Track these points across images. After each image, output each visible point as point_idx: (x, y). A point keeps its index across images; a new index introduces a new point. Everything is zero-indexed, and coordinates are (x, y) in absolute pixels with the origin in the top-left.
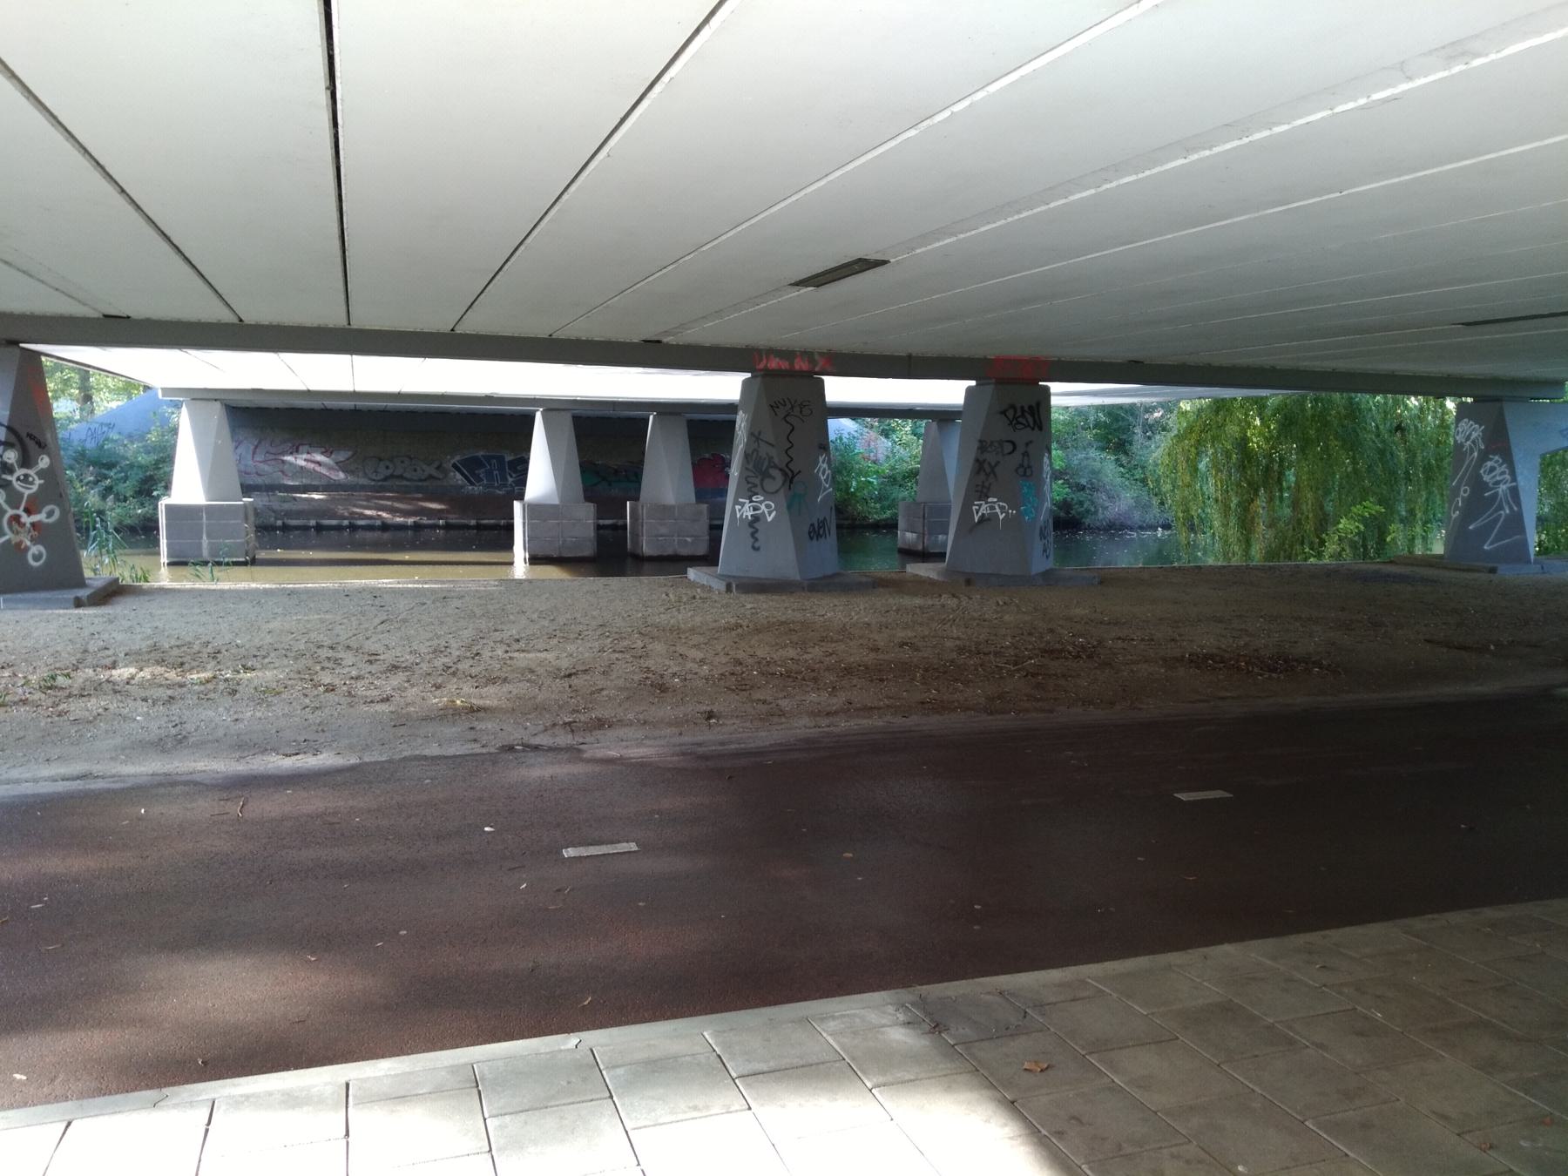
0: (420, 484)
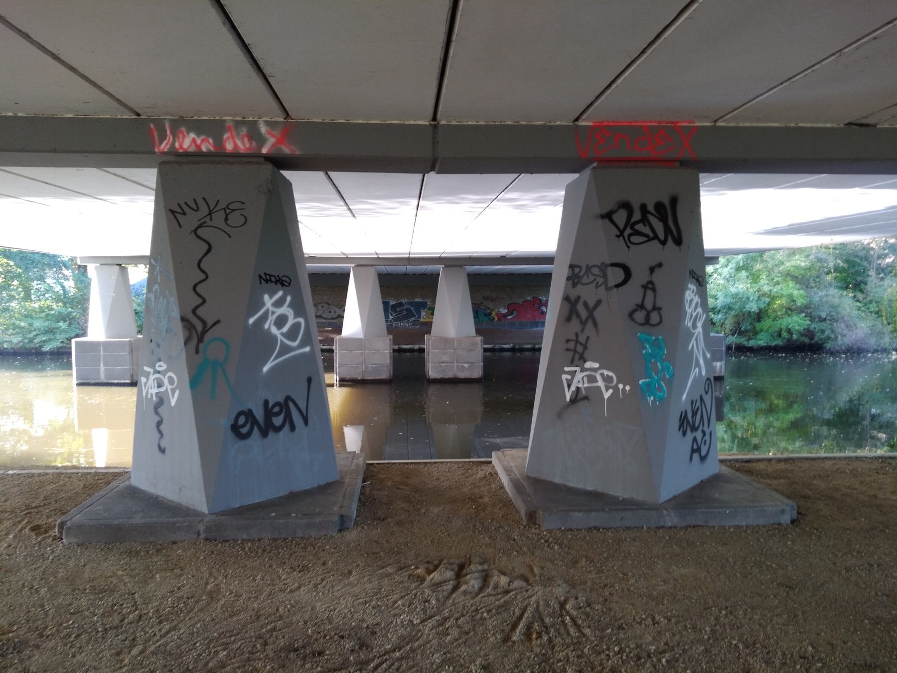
0: (332, 321)
